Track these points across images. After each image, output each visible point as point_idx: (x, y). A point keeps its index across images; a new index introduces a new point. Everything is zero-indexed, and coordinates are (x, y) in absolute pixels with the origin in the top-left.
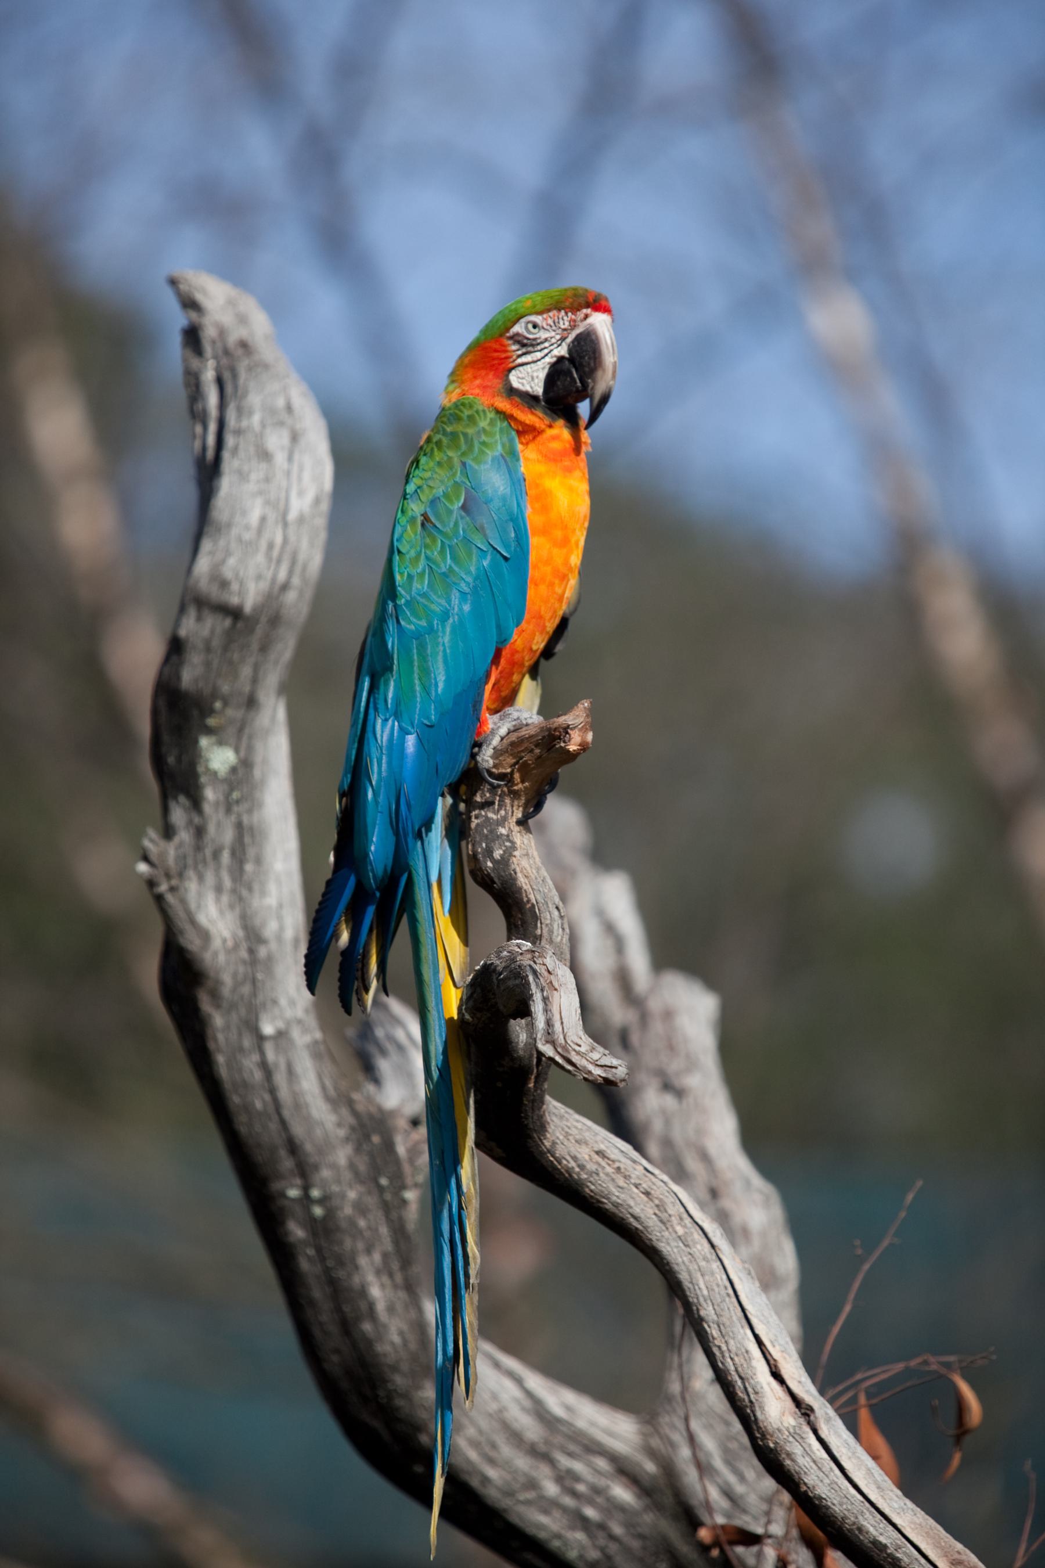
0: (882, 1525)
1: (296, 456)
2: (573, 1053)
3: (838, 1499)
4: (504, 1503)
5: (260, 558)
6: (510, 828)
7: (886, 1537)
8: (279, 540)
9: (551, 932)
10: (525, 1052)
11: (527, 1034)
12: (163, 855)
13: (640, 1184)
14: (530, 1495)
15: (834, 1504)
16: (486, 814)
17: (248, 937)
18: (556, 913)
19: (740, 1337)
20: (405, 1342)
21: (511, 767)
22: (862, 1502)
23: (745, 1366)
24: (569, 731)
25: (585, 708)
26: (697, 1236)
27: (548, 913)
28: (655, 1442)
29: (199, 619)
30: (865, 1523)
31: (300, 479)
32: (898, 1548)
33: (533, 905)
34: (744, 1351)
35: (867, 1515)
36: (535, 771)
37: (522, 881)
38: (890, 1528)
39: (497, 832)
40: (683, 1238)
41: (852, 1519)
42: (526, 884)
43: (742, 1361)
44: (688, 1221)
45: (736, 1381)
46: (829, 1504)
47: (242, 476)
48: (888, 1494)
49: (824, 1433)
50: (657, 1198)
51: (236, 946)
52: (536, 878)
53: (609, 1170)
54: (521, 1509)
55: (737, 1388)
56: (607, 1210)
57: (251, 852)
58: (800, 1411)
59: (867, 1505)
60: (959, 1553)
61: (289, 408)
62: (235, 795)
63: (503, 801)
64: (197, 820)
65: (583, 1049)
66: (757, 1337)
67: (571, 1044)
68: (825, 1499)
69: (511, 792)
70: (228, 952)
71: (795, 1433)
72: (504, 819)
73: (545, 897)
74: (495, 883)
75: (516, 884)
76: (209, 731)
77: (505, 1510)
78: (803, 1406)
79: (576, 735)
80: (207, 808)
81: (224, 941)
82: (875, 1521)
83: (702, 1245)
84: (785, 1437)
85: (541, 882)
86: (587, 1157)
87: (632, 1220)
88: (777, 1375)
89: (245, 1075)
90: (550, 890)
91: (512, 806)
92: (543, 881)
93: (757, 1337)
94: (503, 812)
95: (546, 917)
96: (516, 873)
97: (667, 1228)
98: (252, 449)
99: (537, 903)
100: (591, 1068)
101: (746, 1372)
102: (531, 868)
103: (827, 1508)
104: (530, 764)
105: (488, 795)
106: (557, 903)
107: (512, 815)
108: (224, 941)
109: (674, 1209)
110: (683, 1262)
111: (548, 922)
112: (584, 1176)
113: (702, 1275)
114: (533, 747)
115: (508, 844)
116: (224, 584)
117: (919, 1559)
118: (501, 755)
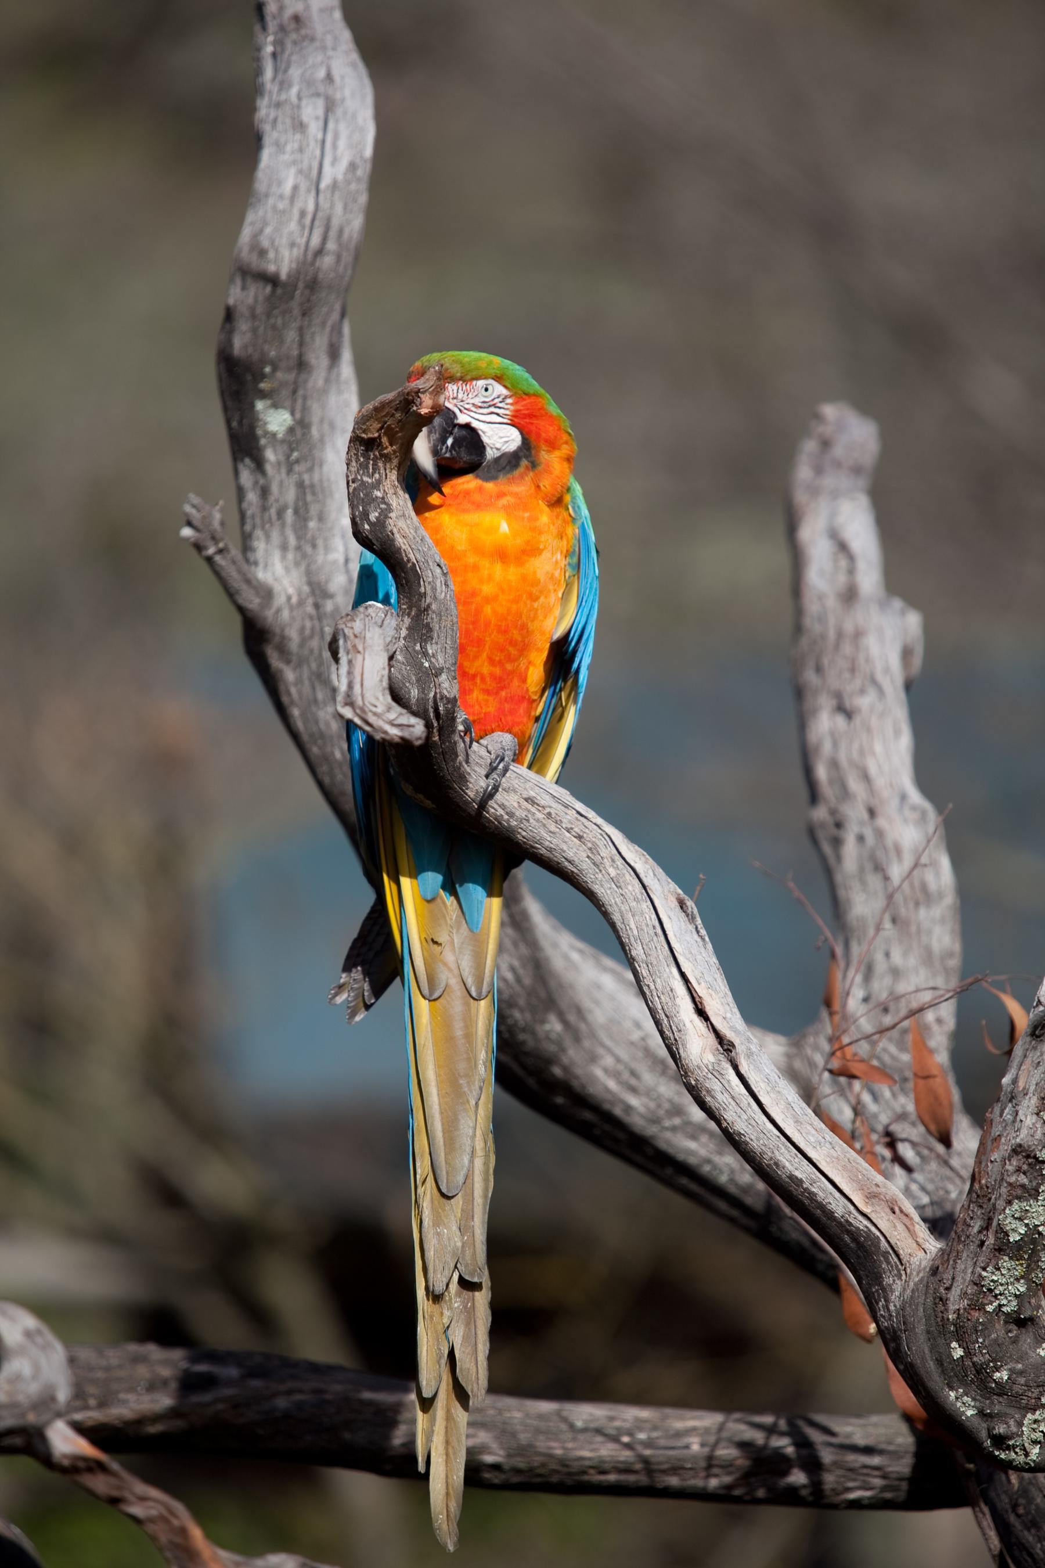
0: (797, 1160)
1: (331, 125)
2: (370, 714)
3: (755, 1135)
4: (651, 1130)
5: (293, 226)
6: (384, 491)
7: (801, 1171)
8: (311, 207)
9: (434, 589)
10: (418, 707)
11: (418, 690)
12: (207, 519)
13: (572, 829)
14: (677, 1121)
15: (752, 1140)
16: (362, 478)
17: (313, 592)
18: (438, 570)
19: (665, 975)
20: (518, 979)
21: (378, 431)
22: (778, 1137)
23: (670, 1004)
24: (420, 394)
25: (436, 371)
26: (629, 877)
27: (429, 571)
28: (798, 1064)
29: (244, 288)
30: (781, 1158)
31: (335, 147)
32: (813, 1182)
33: (414, 564)
34: (669, 989)
35: (783, 1150)
36: (400, 434)
37: (400, 541)
38: (806, 1162)
39: (372, 495)
40: (615, 879)
41: (769, 1154)
42: (404, 544)
43: (668, 999)
44: (620, 862)
45: (663, 1020)
46: (748, 1140)
47: (279, 147)
48: (806, 1128)
49: (744, 1069)
50: (589, 841)
51: (301, 603)
52: (414, 538)
53: (539, 815)
54: (668, 1135)
55: (664, 1026)
56: (542, 855)
57: (314, 510)
58: (722, 1047)
59: (783, 1139)
60: (877, 1185)
61: (329, 78)
62: (295, 454)
63: (376, 465)
64: (262, 481)
65: (379, 710)
66: (683, 975)
67: (368, 705)
68: (743, 1135)
69: (382, 455)
70: (291, 609)
71: (714, 1069)
72: (379, 482)
73: (425, 555)
74: (374, 545)
75: (394, 545)
76: (263, 395)
77: (652, 1137)
78: (725, 1042)
79: (427, 398)
80: (269, 468)
81: (289, 598)
82: (791, 1156)
83: (633, 886)
84: (705, 1074)
85: (420, 542)
86: (516, 805)
87: (566, 863)
88: (701, 1013)
89: (322, 726)
90: (429, 549)
91: (385, 470)
92: (421, 540)
93: (683, 975)
94: (377, 476)
95: (427, 576)
96: (393, 534)
97: (600, 871)
98: (288, 121)
99: (417, 562)
100: (388, 728)
101: (671, 1011)
102: (409, 528)
103: (747, 1143)
104: (393, 429)
105: (362, 459)
106: (438, 561)
107: (386, 478)
108: (289, 598)
109: (607, 852)
110: (616, 903)
111: (430, 579)
112: (514, 823)
113: (633, 916)
114: (393, 411)
115: (383, 506)
116: (262, 253)
117: (833, 1193)
118: (368, 420)
